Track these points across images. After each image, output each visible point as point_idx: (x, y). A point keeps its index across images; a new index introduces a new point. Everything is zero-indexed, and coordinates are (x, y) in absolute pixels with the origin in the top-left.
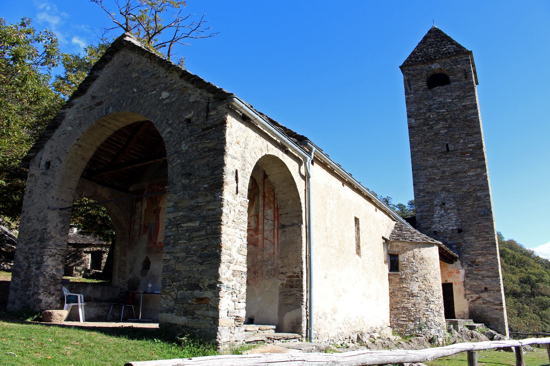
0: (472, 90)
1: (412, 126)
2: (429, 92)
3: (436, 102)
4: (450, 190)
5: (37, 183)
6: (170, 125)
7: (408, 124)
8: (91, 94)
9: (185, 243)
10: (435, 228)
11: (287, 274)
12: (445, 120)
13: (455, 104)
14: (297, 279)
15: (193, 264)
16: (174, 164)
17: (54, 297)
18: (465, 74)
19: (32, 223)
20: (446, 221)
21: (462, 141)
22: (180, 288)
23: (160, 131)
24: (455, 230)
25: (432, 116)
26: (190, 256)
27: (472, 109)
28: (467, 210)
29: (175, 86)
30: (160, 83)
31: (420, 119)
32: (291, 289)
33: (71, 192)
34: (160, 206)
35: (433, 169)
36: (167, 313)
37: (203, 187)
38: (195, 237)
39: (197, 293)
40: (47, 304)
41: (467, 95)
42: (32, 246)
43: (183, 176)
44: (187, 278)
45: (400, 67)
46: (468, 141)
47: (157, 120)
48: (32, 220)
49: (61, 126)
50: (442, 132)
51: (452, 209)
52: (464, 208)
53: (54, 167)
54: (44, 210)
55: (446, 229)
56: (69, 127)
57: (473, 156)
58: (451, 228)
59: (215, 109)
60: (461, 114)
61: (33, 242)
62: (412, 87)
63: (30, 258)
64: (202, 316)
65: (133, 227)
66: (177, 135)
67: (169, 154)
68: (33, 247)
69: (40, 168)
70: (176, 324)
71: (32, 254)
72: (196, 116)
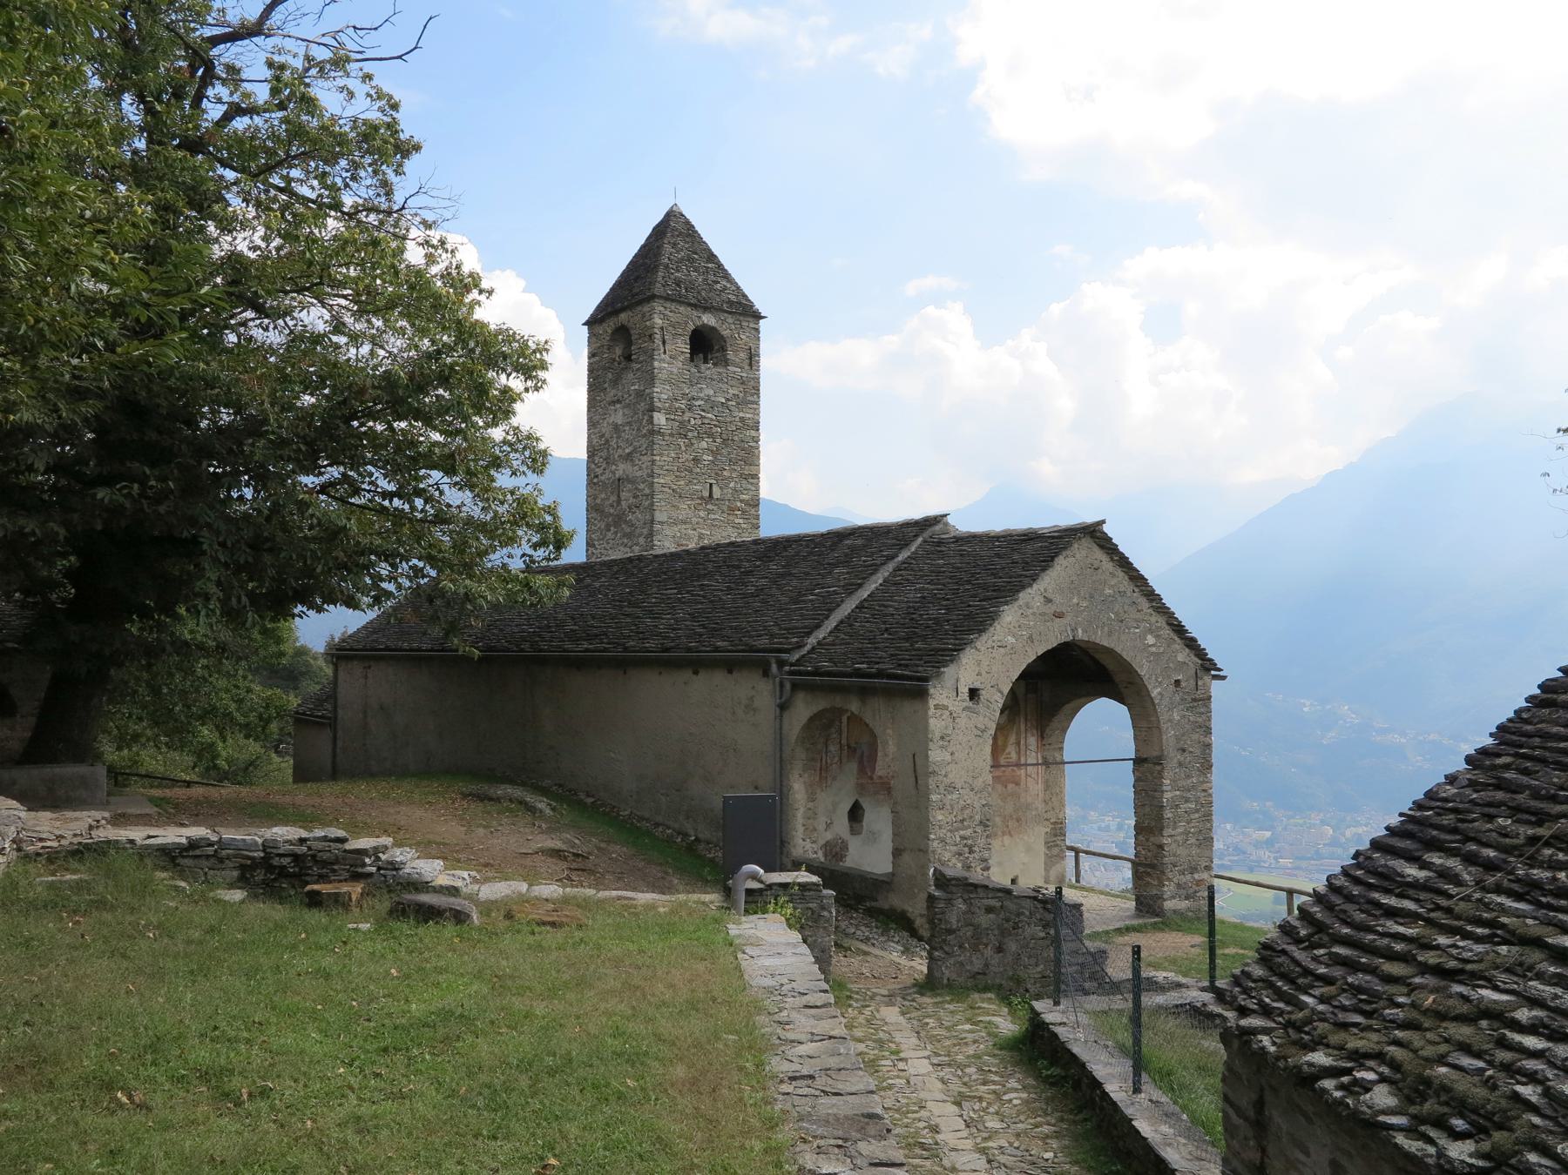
3: (702, 395)
12: (711, 435)
23: (1150, 687)
25: (693, 422)
50: (705, 457)
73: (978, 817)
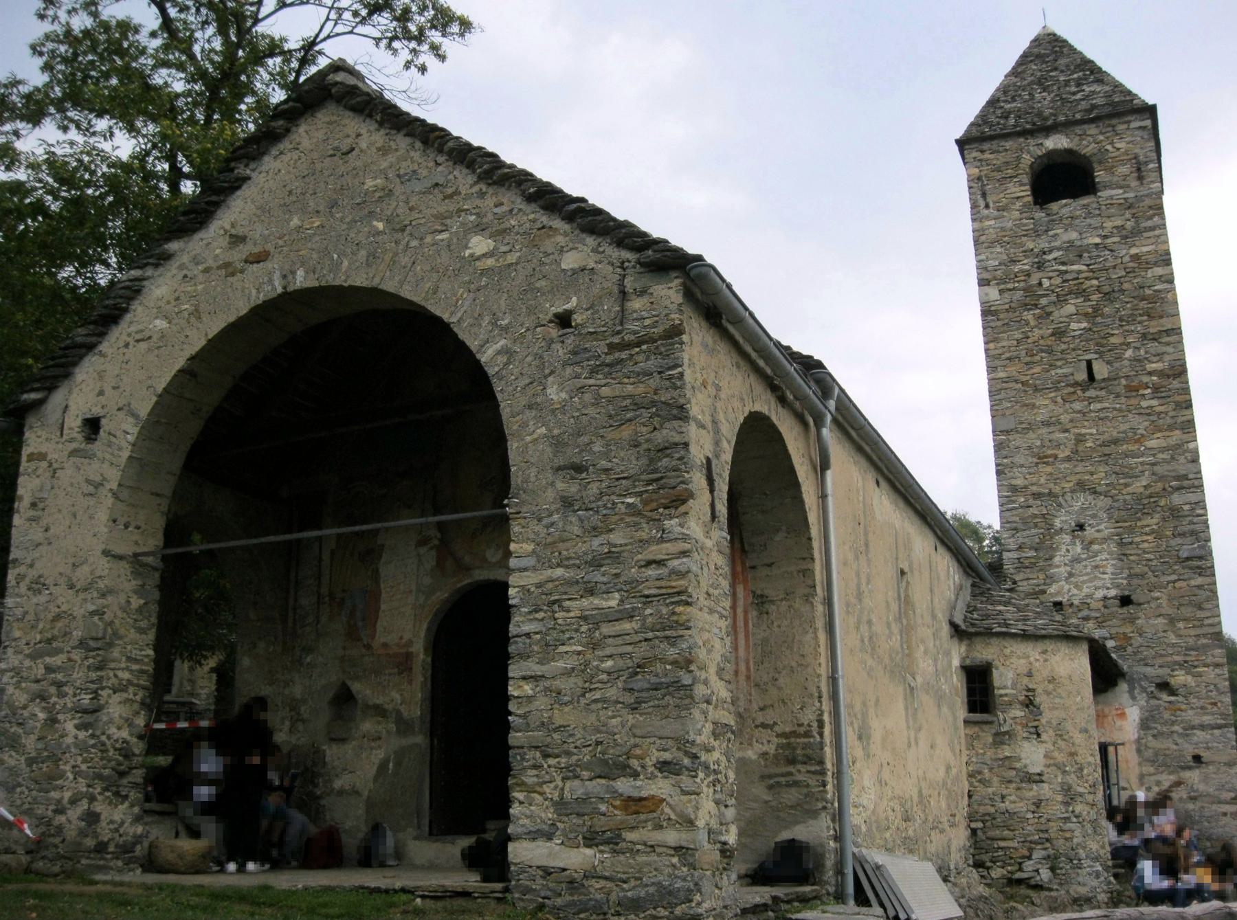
0: (1159, 215)
1: (993, 308)
2: (1040, 215)
3: (1057, 244)
4: (1099, 489)
5: (58, 478)
6: (505, 329)
7: (982, 303)
8: (228, 227)
9: (579, 653)
10: (1058, 593)
11: (777, 728)
12: (1082, 293)
13: (1111, 251)
14: (806, 740)
15: (606, 708)
16: (529, 439)
17: (126, 804)
18: (1139, 170)
19: (50, 594)
20: (1087, 574)
21: (1129, 353)
22: (571, 773)
23: (473, 344)
24: (1112, 598)
25: (1046, 283)
26: (596, 686)
27: (1156, 264)
28: (1145, 545)
29: (513, 222)
30: (460, 211)
31: (1014, 289)
32: (791, 769)
33: (160, 505)
34: (379, 542)
35: (1052, 428)
36: (534, 839)
37: (623, 503)
38: (610, 637)
39: (624, 785)
40: (112, 826)
41: (1143, 225)
42: (57, 660)
43: (560, 472)
44: (590, 745)
45: (957, 141)
46: (1146, 353)
47: (459, 315)
48: (52, 588)
49: (128, 317)
50: (1074, 326)
51: (1105, 540)
52: (1137, 539)
53: (115, 436)
54: (91, 560)
55: (1090, 596)
56: (158, 322)
57: (1159, 395)
58: (1100, 594)
59: (643, 293)
60: (1127, 279)
61: (58, 651)
62: (990, 200)
63: (50, 696)
64: (645, 844)
65: (296, 600)
66: (529, 359)
67: (508, 410)
68: (59, 663)
69: (65, 437)
70: (564, 870)
71: (59, 685)
72: (587, 310)
73: (77, 634)
